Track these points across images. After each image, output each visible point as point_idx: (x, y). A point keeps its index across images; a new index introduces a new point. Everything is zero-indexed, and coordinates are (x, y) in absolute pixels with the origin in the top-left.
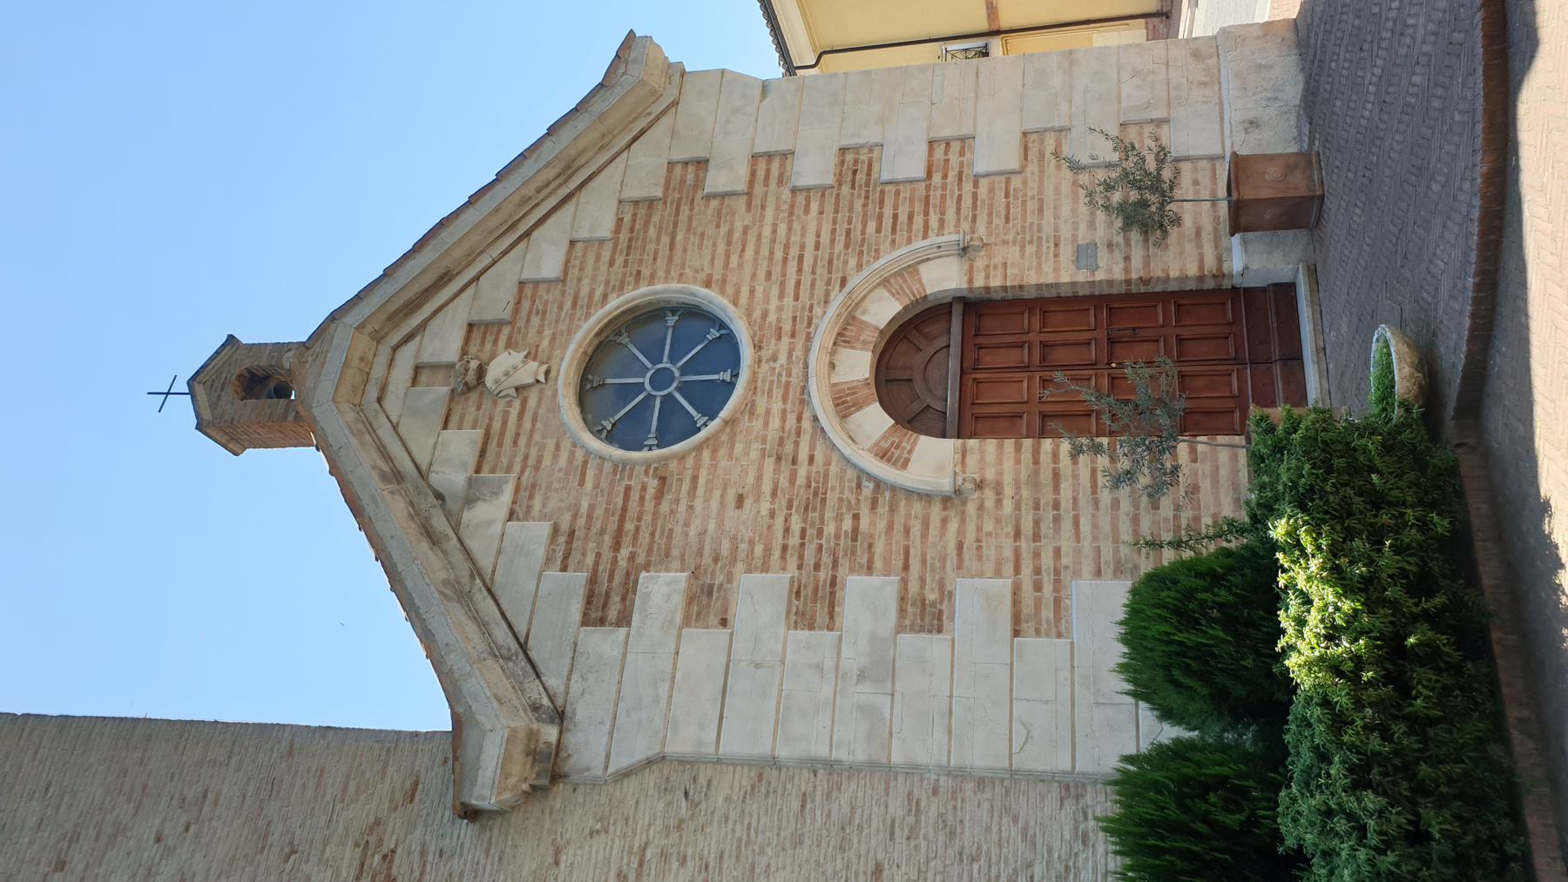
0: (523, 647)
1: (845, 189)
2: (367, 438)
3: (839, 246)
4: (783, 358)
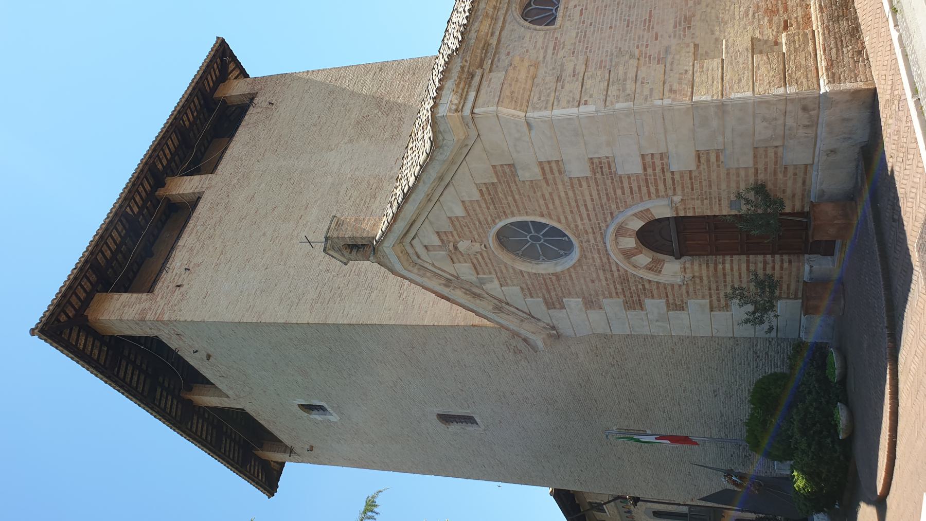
0: (530, 314)
1: (599, 176)
2: (428, 274)
3: (604, 200)
4: (592, 241)
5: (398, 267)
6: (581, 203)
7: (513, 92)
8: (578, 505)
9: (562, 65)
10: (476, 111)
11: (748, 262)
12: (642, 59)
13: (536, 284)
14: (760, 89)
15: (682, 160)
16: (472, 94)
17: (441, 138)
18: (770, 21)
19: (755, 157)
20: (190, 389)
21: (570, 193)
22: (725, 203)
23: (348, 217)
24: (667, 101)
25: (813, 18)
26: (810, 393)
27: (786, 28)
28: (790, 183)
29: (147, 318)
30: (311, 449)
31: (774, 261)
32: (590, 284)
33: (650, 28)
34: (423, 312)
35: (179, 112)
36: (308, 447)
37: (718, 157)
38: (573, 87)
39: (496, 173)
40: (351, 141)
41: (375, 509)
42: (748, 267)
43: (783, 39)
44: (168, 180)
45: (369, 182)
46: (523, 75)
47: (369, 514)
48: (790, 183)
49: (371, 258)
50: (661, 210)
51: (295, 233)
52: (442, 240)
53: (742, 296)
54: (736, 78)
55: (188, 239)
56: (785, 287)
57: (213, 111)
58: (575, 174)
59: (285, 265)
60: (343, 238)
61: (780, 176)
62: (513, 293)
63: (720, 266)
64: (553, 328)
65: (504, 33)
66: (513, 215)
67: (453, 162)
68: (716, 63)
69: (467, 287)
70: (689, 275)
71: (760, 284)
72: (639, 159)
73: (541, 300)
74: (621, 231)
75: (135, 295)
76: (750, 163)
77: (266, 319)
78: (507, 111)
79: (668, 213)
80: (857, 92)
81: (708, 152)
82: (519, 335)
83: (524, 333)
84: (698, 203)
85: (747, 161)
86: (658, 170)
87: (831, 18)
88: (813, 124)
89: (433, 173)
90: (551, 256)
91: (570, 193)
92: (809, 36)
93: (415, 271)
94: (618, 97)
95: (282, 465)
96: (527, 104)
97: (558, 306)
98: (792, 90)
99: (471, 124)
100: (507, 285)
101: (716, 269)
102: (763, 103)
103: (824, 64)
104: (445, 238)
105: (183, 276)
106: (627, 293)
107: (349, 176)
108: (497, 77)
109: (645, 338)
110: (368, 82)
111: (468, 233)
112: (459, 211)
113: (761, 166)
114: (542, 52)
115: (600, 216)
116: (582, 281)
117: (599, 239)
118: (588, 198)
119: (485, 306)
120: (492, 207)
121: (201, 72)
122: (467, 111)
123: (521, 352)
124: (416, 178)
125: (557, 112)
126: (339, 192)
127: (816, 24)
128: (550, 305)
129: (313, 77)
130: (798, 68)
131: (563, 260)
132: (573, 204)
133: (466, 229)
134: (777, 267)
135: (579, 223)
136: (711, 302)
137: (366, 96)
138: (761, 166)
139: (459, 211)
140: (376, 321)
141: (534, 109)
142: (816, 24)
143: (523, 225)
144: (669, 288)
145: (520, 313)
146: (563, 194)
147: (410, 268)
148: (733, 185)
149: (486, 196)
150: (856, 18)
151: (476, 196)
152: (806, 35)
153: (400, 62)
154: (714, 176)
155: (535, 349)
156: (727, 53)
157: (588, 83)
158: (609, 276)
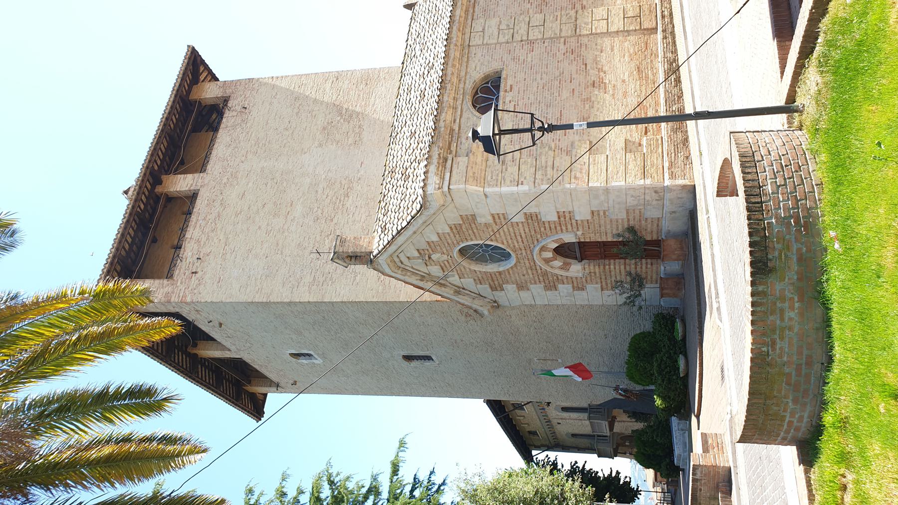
1: (530, 221)
3: (533, 233)
5: (388, 271)
6: (518, 234)
11: (625, 264)
15: (582, 213)
16: (448, 175)
19: (627, 213)
20: (195, 345)
21: (511, 229)
23: (349, 235)
28: (649, 226)
29: (172, 300)
30: (295, 383)
35: (167, 119)
36: (292, 382)
37: (604, 213)
40: (320, 145)
43: (644, 142)
44: (164, 177)
48: (649, 226)
50: (569, 238)
51: (286, 227)
52: (420, 253)
54: (615, 170)
55: (194, 232)
56: (649, 277)
57: (194, 117)
59: (282, 254)
60: (347, 252)
62: (469, 283)
64: (495, 302)
66: (472, 240)
70: (587, 271)
71: (633, 280)
73: (487, 286)
75: (157, 281)
76: (625, 217)
77: (274, 298)
78: (472, 188)
79: (574, 240)
80: (684, 187)
82: (471, 308)
83: (474, 306)
88: (662, 199)
89: (420, 221)
90: (493, 260)
91: (511, 229)
92: (660, 142)
93: (400, 272)
94: (542, 180)
95: (265, 395)
98: (648, 182)
102: (629, 189)
105: (196, 264)
106: (547, 282)
107: (323, 177)
108: (462, 161)
110: (327, 90)
112: (435, 238)
113: (631, 218)
115: (530, 241)
119: (448, 292)
121: (179, 80)
122: (446, 189)
125: (505, 189)
128: (494, 289)
129: (278, 83)
130: (652, 165)
131: (504, 263)
132: (513, 235)
134: (644, 267)
135: (516, 244)
139: (435, 238)
140: (362, 299)
141: (489, 185)
148: (614, 226)
151: (448, 230)
152: (657, 140)
154: (602, 222)
157: (523, 167)
158: (535, 272)
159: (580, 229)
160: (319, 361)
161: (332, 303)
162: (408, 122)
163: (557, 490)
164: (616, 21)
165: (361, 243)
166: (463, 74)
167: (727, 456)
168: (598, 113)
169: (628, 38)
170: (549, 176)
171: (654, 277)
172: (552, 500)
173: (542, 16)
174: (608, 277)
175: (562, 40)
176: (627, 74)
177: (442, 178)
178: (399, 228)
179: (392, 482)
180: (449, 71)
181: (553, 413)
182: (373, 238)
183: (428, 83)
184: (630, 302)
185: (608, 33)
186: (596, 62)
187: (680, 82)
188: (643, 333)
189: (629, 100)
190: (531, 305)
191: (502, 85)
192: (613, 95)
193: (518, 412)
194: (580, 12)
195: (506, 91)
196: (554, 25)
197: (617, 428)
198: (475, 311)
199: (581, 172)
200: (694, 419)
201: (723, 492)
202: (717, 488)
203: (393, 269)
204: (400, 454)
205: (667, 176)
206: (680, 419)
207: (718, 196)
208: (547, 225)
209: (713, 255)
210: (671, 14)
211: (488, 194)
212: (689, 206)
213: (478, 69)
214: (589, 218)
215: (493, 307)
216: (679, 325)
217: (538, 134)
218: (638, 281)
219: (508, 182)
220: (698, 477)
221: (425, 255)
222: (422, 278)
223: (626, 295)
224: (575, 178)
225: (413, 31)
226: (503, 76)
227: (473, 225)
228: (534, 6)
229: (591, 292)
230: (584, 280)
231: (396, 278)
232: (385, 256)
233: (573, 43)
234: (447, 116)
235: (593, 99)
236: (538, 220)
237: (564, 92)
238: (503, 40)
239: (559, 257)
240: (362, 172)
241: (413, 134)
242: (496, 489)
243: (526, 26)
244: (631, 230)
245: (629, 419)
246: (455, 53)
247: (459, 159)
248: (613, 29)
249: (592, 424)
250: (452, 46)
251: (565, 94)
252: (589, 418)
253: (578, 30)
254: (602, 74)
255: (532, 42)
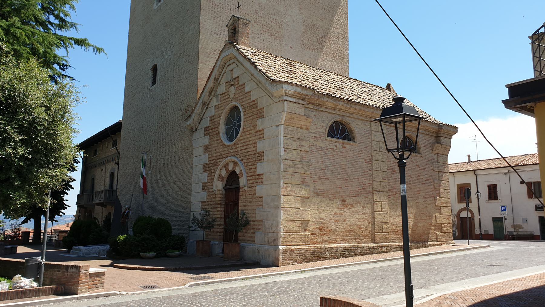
0: (202, 119)
1: (257, 155)
2: (220, 70)
3: (248, 157)
4: (232, 151)
5: (224, 55)
7: (294, 119)
8: (115, 134)
9: (306, 140)
10: (286, 102)
11: (221, 218)
12: (304, 175)
13: (215, 123)
14: (284, 223)
15: (260, 190)
16: (294, 100)
17: (275, 85)
18: (317, 228)
19: (259, 221)
21: (251, 142)
22: (243, 208)
24: (282, 185)
25: (315, 245)
26: (162, 243)
27: (312, 234)
28: (249, 235)
31: (220, 229)
32: (214, 149)
33: (320, 179)
34: (205, 63)
37: (260, 205)
38: (294, 145)
39: (261, 109)
40: (304, 21)
41: (98, 53)
42: (218, 218)
45: (279, 32)
46: (302, 123)
47: (96, 50)
48: (249, 235)
49: (228, 41)
50: (243, 181)
52: (235, 79)
53: (206, 215)
56: (210, 233)
58: (258, 145)
61: (252, 231)
62: (211, 111)
63: (219, 206)
64: (196, 130)
65: (326, 114)
66: (244, 115)
67: (266, 89)
68: (298, 205)
69: (215, 89)
70: (217, 193)
71: (210, 223)
72: (261, 173)
73: (208, 125)
74: (235, 163)
76: (257, 219)
78: (284, 116)
81: (262, 201)
82: (192, 113)
83: (193, 115)
84: (244, 197)
85: (258, 218)
86: (257, 180)
87: (314, 252)
88: (269, 244)
89: (262, 79)
90: (227, 131)
91: (251, 142)
92: (307, 243)
93: (222, 63)
94: (287, 165)
96: (287, 124)
97: (206, 133)
98: (282, 235)
99: (280, 99)
100: (215, 109)
101: (218, 204)
103: (293, 248)
104: (236, 80)
106: (210, 165)
107: (284, 21)
108: (302, 111)
109: (191, 172)
110: (337, 30)
111: (238, 92)
112: (247, 89)
113: (256, 223)
114: (314, 131)
115: (242, 155)
116: (216, 145)
117: (233, 154)
118: (248, 150)
119: (205, 97)
120: (248, 105)
122: (285, 98)
123: (186, 112)
124: (260, 70)
125: (282, 139)
126: (274, 15)
127: (312, 246)
128: (206, 129)
130: (292, 238)
131: (225, 137)
132: (247, 143)
133: (239, 91)
134: (218, 230)
135: (240, 145)
136: (205, 202)
137: (329, 29)
138: (256, 223)
139: (247, 89)
140: (201, 37)
141: (285, 128)
142: (312, 246)
143: (240, 120)
144: (211, 184)
145: (202, 114)
146: (251, 139)
147: (223, 61)
148: (250, 212)
149: (252, 103)
150: (312, 261)
151: (253, 98)
152: (308, 242)
153: (347, 48)
154: (253, 204)
155: (186, 120)
156: (303, 210)
157: (295, 152)
158: (218, 157)
159: (249, 189)
160: (155, 6)
161: (199, 16)
162: (323, 79)
163: (62, 162)
164: (381, 217)
165: (244, 37)
166: (355, 116)
167: (86, 292)
168: (326, 203)
169: (370, 225)
170: (289, 169)
171: (210, 237)
172: (54, 157)
173: (386, 170)
174: (211, 207)
175: (371, 182)
176: (349, 222)
177: (292, 96)
178: (256, 64)
179: (70, 39)
180: (357, 107)
181: (111, 166)
182: (247, 47)
183: (348, 93)
184: (195, 220)
185: (373, 211)
186: (357, 203)
187: (343, 257)
188: (171, 229)
189: (333, 224)
190: (192, 154)
191: (346, 141)
192: (337, 213)
193: (111, 144)
194: (387, 194)
195: (343, 144)
196: (380, 177)
197: (98, 209)
198: (190, 116)
199: (290, 191)
200: (109, 262)
201: (56, 288)
202: (59, 284)
203: (225, 59)
204: (91, 48)
205: (285, 247)
206: (107, 251)
207: (322, 299)
208: (253, 167)
209: (235, 280)
210: (383, 252)
211: (279, 127)
212: (263, 262)
213: (357, 126)
214: (257, 195)
215: (192, 128)
216: (176, 253)
217: (397, 155)
218: (208, 226)
219: (286, 142)
220: (70, 270)
221: (234, 82)
222: (216, 79)
223: (199, 218)
224: (287, 187)
225: (375, 88)
226: (352, 143)
227: (256, 116)
228: (392, 165)
229: (200, 193)
230: (211, 190)
231: (217, 61)
232: (236, 54)
233: (369, 189)
234: (330, 104)
235: (335, 200)
236: (257, 161)
237: (340, 182)
238: (373, 144)
239: (228, 174)
240: (285, 47)
241: (316, 80)
242: (65, 113)
243: (380, 159)
244: (247, 223)
245: (104, 216)
246: (368, 112)
247: (303, 109)
248: (376, 215)
249: (102, 191)
250: (372, 110)
251: (339, 182)
252: (106, 190)
253: (376, 192)
254: (349, 207)
255: (371, 162)
